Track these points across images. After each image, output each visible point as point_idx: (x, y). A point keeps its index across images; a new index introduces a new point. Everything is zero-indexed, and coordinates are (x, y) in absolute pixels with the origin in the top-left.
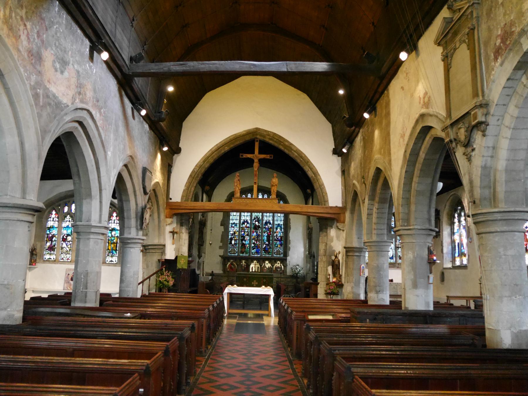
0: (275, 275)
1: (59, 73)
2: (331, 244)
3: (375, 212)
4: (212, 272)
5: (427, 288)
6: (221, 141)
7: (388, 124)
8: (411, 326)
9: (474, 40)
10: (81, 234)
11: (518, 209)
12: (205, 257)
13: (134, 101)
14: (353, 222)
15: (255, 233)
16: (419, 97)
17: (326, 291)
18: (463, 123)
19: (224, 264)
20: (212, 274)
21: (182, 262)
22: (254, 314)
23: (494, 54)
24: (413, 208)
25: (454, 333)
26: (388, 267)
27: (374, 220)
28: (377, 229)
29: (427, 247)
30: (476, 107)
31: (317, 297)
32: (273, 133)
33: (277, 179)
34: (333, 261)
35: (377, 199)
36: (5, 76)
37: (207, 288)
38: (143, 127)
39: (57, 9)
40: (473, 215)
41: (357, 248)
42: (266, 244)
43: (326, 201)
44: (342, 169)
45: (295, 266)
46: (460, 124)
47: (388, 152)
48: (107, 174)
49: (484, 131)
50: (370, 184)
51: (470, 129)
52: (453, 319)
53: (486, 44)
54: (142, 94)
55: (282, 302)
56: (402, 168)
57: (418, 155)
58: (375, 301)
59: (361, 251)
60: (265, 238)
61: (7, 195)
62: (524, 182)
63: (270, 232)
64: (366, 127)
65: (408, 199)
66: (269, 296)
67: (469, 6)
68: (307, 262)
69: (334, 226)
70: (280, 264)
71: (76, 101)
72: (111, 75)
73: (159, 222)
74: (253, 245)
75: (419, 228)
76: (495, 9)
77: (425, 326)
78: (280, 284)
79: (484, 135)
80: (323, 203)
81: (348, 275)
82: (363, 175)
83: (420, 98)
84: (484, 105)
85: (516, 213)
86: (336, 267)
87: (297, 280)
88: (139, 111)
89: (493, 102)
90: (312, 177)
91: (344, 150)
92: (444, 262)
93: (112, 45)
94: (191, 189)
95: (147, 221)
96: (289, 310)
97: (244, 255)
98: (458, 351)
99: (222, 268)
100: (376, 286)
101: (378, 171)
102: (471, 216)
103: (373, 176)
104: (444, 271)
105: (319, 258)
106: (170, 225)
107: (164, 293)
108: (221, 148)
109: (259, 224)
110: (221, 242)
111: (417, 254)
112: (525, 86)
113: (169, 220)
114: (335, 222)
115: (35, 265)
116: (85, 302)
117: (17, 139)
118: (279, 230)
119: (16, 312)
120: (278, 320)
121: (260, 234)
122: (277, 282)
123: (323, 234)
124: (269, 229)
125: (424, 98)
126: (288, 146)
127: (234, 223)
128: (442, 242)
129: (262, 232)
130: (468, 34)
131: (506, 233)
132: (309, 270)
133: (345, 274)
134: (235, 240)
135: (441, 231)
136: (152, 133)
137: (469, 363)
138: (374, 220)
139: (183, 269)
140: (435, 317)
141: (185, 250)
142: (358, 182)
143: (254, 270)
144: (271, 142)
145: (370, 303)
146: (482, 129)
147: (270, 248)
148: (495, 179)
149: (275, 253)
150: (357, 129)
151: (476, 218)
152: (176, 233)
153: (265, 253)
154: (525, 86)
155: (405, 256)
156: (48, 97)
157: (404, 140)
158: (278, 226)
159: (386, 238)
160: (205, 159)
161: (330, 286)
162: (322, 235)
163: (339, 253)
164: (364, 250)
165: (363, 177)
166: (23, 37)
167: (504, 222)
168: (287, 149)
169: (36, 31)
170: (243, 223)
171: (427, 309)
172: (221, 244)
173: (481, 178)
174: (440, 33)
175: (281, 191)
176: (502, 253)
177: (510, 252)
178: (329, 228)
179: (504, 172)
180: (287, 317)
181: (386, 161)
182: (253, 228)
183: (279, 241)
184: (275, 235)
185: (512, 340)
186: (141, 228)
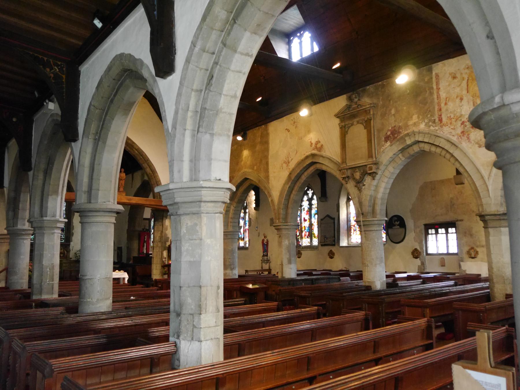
3: (233, 210)
16: (311, 142)
27: (231, 215)
28: (233, 222)
35: (236, 200)
53: (379, 131)
61: (109, 201)
75: (294, 224)
84: (376, 164)
85: (191, 201)
89: (382, 163)
137: (237, 317)
174: (340, 112)
176: (376, 241)
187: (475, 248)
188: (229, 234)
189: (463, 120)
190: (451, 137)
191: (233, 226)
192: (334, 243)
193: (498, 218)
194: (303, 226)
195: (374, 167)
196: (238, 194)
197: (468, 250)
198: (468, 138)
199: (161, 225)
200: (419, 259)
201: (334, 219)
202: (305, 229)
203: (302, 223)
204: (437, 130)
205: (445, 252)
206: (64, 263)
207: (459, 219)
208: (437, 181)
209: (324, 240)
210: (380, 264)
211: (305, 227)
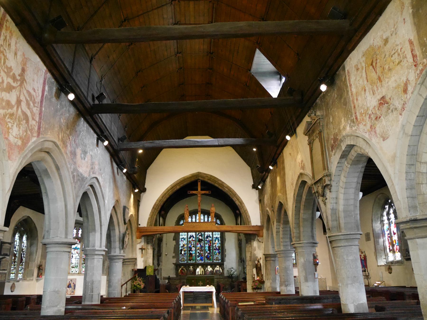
0: (215, 276)
1: (83, 160)
2: (255, 252)
3: (281, 231)
4: (169, 276)
5: (314, 281)
6: (174, 182)
7: (284, 174)
9: (322, 138)
10: (89, 255)
11: (352, 233)
12: (162, 265)
13: (119, 163)
14: (268, 236)
15: (199, 245)
17: (252, 287)
18: (320, 183)
19: (177, 270)
20: (169, 278)
21: (150, 270)
22: (201, 307)
23: (331, 148)
29: (312, 254)
30: (324, 176)
31: (246, 291)
32: (210, 175)
33: (214, 208)
36: (60, 169)
37: (166, 289)
38: (123, 178)
39: (82, 123)
42: (208, 253)
43: (249, 222)
45: (231, 269)
47: (285, 192)
48: (105, 215)
49: (330, 189)
51: (323, 187)
52: (328, 300)
54: (124, 159)
55: (222, 296)
56: (293, 204)
57: (302, 196)
60: (207, 248)
61: (57, 237)
63: (210, 244)
64: (272, 173)
66: (212, 292)
67: (317, 120)
68: (239, 266)
69: (256, 239)
70: (219, 268)
71: (91, 174)
72: (107, 151)
73: (132, 242)
74: (198, 254)
76: (329, 124)
78: (219, 284)
79: (330, 192)
80: (247, 223)
83: (299, 163)
84: (329, 175)
86: (258, 269)
87: (232, 280)
88: (122, 170)
90: (239, 205)
91: (260, 187)
93: (109, 135)
94: (154, 217)
95: (127, 243)
96: (227, 301)
97: (192, 262)
98: (323, 316)
99: (175, 273)
101: (281, 205)
103: (278, 207)
105: (247, 263)
106: (140, 244)
107: (137, 294)
108: (174, 187)
109: (202, 238)
110: (174, 253)
111: (306, 259)
112: (346, 166)
113: (139, 240)
115: (41, 277)
116: (92, 302)
117: (63, 203)
118: (217, 241)
119: (62, 308)
120: (219, 309)
121: (203, 245)
122: (217, 282)
123: (248, 246)
124: (209, 241)
125: (301, 164)
126: (221, 184)
127: (183, 238)
129: (204, 244)
130: (319, 134)
132: (241, 272)
133: (265, 273)
134: (184, 251)
136: (128, 181)
138: (281, 236)
139: (151, 276)
141: (150, 261)
143: (199, 274)
144: (209, 181)
145: (282, 293)
146: (329, 188)
147: (211, 256)
149: (215, 259)
150: (267, 174)
152: (144, 249)
153: (207, 259)
154: (346, 166)
155: (299, 261)
156: (78, 175)
158: (216, 239)
159: (290, 248)
160: (163, 195)
161: (255, 283)
162: (248, 246)
163: (260, 258)
165: (272, 207)
166: (69, 145)
168: (220, 186)
169: (73, 139)
170: (190, 238)
172: (174, 255)
175: (218, 212)
176: (346, 258)
177: (350, 258)
178: (252, 241)
180: (226, 305)
182: (198, 241)
183: (217, 250)
184: (214, 246)
185: (355, 309)
186: (123, 248)
189: (369, 113)
190: (364, 134)
194: (394, 240)
195: (327, 179)
198: (375, 132)
199: (250, 247)
202: (396, 243)
203: (392, 237)
204: (356, 130)
206: (216, 278)
209: (407, 254)
210: (352, 284)
211: (395, 240)
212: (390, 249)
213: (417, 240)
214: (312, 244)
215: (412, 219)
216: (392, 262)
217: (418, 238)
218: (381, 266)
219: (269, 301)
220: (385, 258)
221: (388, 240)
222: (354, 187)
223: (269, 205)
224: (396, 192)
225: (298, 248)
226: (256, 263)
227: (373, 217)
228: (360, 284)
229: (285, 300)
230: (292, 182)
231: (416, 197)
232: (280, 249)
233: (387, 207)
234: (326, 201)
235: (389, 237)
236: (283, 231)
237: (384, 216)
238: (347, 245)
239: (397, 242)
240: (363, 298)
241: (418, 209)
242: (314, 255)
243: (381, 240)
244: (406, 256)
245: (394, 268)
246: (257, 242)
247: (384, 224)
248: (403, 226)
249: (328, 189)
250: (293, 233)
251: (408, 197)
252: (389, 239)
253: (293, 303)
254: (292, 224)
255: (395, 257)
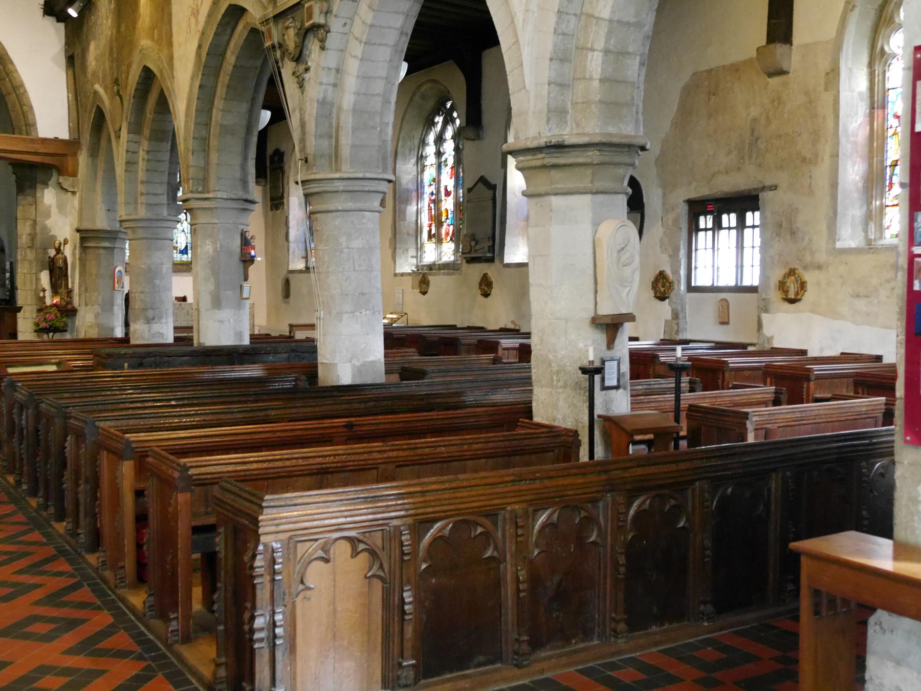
3: (143, 160)
5: (239, 306)
8: (202, 369)
11: (368, 175)
14: (95, 173)
17: (37, 324)
18: (293, 18)
24: (214, 157)
25: (274, 373)
26: (171, 270)
27: (141, 175)
28: (148, 194)
34: (52, 261)
40: (302, 182)
41: (108, 232)
43: (30, 125)
44: (66, 51)
46: (288, 19)
47: (165, 39)
49: (322, 40)
50: (132, 100)
51: (303, 32)
52: (278, 356)
56: (192, 79)
57: (223, 55)
58: (143, 338)
59: (116, 239)
62: (381, 131)
65: (205, 139)
75: (225, 197)
77: (228, 368)
79: (323, 48)
80: (24, 128)
81: (86, 289)
82: (115, 76)
86: (58, 272)
91: (72, 12)
92: (290, 259)
100: (146, 309)
101: (148, 76)
102: (300, 183)
103: (138, 83)
104: (291, 276)
111: (221, 246)
114: (55, 174)
128: (287, 218)
131: (351, 213)
133: (80, 286)
135: (285, 195)
138: (141, 175)
140: (248, 354)
142: (106, 91)
148: (338, 123)
151: (308, 186)
157: (197, 21)
159: (165, 213)
163: (66, 241)
164: (121, 236)
165: (116, 82)
167: (348, 195)
171: (237, 343)
173: (316, 120)
176: (344, 244)
177: (357, 244)
179: (351, 113)
181: (164, 56)
185: (353, 376)
187: (800, 271)
188: (136, 227)
191: (149, 205)
192: (489, 255)
193: (539, 163)
194: (443, 209)
196: (148, 115)
197: (780, 278)
200: (667, 301)
201: (493, 188)
202: (447, 219)
205: (732, 283)
207: (768, 183)
208: (724, 66)
209: (471, 246)
211: (447, 211)
212: (430, 231)
213: (553, 198)
214: (242, 202)
215: (552, 144)
216: (431, 267)
217: (555, 194)
218: (402, 275)
219: (103, 361)
220: (415, 254)
221: (430, 209)
222: (392, 43)
223: (104, 77)
224: (522, 64)
225: (199, 212)
226: (52, 255)
227: (400, 144)
228: (374, 313)
229: (155, 356)
230: (194, 7)
231: (569, 86)
232: (137, 214)
233: (439, 119)
234: (307, 76)
235: (434, 201)
236: (148, 161)
237: (428, 144)
238: (353, 208)
239: (450, 216)
240: (376, 351)
241: (569, 117)
242: (243, 235)
243: (412, 209)
244: (469, 252)
245: (435, 280)
246: (54, 191)
247: (424, 166)
248: (523, 161)
249: (316, 40)
250: (188, 167)
251: (552, 83)
252: (433, 208)
253: (181, 365)
254: (185, 140)
255: (441, 253)
